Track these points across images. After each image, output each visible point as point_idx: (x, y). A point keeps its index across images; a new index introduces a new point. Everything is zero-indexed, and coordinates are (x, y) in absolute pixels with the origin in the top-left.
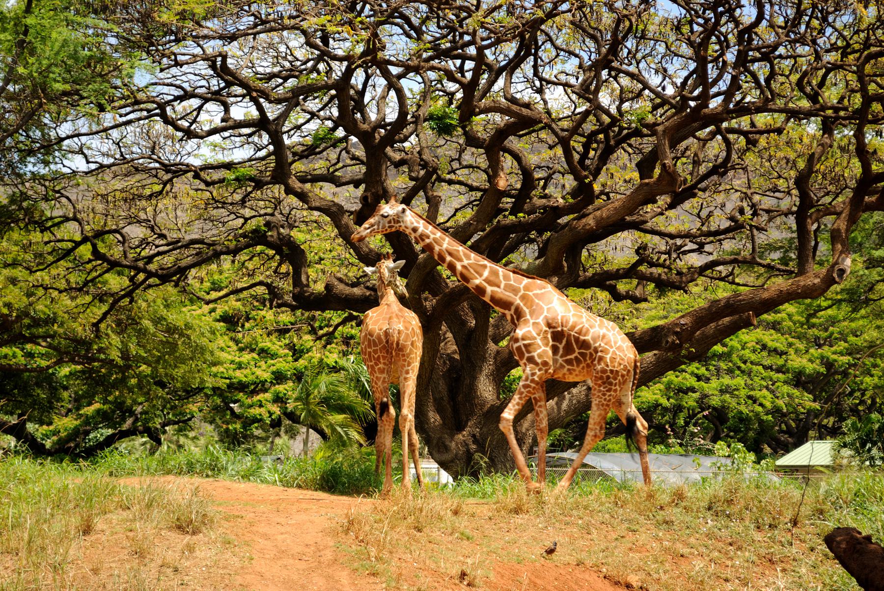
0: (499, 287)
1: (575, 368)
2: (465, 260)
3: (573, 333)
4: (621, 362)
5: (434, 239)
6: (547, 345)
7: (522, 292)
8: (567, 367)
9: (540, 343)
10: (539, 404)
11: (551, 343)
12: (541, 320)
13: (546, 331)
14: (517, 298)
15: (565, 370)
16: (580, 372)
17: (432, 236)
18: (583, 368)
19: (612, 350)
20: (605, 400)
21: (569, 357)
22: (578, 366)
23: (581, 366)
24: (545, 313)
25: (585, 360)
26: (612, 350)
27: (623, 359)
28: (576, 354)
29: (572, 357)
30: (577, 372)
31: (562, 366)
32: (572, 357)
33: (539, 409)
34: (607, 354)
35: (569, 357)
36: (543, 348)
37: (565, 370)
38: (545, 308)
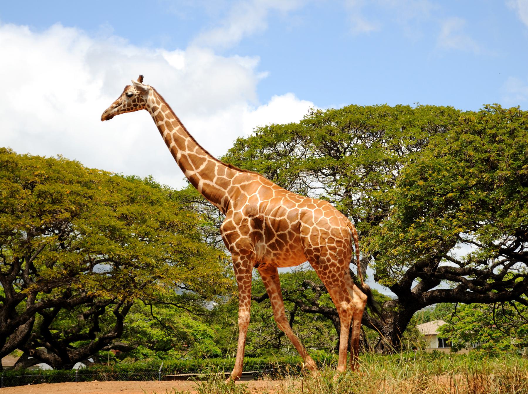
0: (212, 181)
1: (279, 252)
2: (187, 150)
3: (269, 217)
4: (324, 236)
5: (167, 123)
6: (246, 233)
7: (231, 185)
8: (273, 252)
9: (239, 232)
10: (273, 296)
11: (251, 230)
12: (241, 211)
13: (245, 220)
14: (226, 191)
15: (272, 255)
16: (285, 255)
17: (166, 119)
18: (287, 251)
19: (311, 228)
20: (329, 277)
21: (271, 242)
22: (281, 249)
23: (284, 249)
24: (247, 203)
25: (287, 242)
26: (311, 228)
27: (326, 233)
28: (276, 237)
29: (273, 241)
30: (283, 256)
31: (268, 252)
32: (273, 241)
33: (274, 301)
34: (307, 234)
35: (271, 242)
36: (241, 236)
37: (272, 255)
38: (248, 197)
